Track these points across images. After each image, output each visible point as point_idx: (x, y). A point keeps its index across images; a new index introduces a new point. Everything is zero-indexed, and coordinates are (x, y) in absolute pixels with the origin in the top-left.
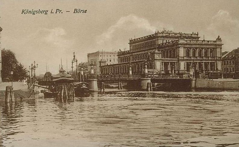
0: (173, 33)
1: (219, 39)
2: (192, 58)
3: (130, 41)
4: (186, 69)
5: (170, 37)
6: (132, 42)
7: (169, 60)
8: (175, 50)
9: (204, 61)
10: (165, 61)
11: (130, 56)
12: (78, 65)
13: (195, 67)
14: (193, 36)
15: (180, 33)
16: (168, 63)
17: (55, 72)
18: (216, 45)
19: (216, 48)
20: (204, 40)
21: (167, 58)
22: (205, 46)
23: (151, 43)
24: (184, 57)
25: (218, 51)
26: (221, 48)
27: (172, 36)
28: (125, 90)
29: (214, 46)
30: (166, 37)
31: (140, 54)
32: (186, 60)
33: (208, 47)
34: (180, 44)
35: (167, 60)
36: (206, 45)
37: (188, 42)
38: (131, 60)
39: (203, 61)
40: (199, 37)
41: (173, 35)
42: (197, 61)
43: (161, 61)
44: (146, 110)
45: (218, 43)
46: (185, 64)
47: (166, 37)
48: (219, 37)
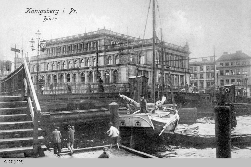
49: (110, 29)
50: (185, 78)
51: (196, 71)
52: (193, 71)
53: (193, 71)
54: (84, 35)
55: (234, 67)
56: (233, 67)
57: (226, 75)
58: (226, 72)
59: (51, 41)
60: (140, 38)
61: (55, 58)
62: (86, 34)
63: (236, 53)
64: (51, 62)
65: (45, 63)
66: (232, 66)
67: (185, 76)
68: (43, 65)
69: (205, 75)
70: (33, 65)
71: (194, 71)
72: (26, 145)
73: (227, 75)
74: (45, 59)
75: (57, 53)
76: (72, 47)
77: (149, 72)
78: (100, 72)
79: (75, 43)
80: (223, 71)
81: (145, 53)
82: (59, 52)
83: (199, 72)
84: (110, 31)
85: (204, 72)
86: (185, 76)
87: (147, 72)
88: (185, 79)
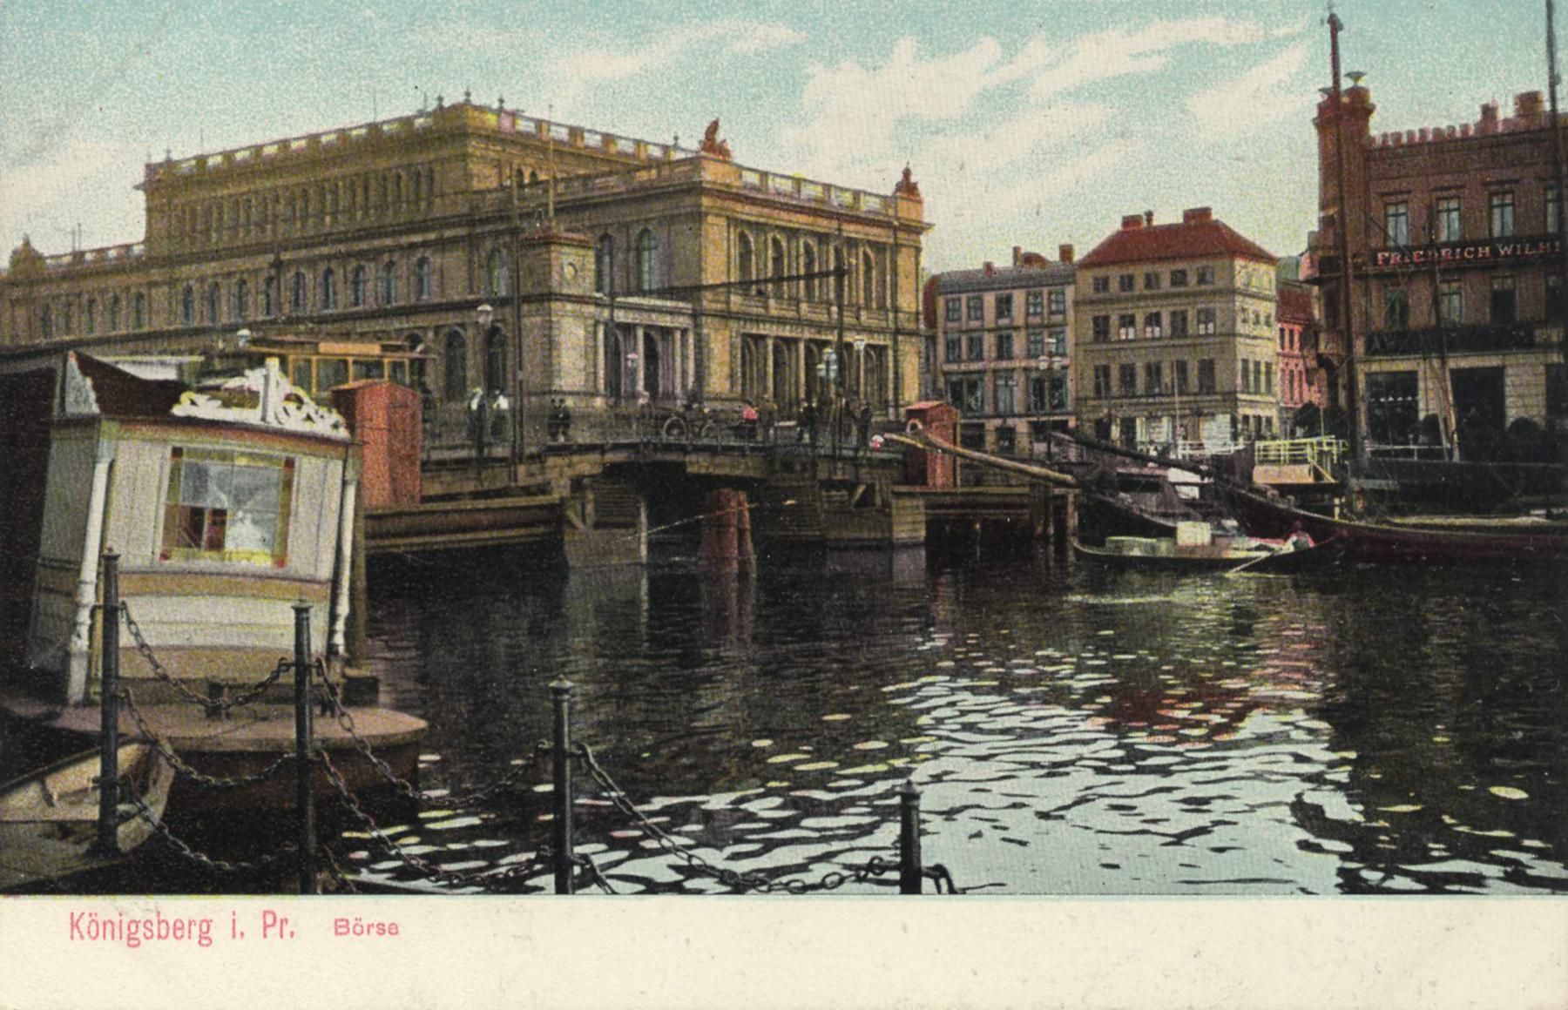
19: (896, 247)
26: (918, 250)
45: (905, 211)
48: (907, 173)
49: (501, 101)
50: (896, 361)
51: (1058, 312)
52: (964, 318)
53: (964, 318)
54: (369, 133)
55: (1214, 293)
56: (1153, 297)
57: (1146, 339)
58: (1123, 325)
59: (201, 160)
60: (676, 147)
61: (215, 256)
62: (374, 128)
63: (1181, 220)
64: (202, 279)
65: (172, 283)
66: (1203, 287)
67: (896, 351)
68: (159, 294)
69: (1019, 343)
70: (86, 297)
71: (1051, 313)
72: (597, 853)
73: (1128, 341)
74: (172, 261)
75: (234, 229)
76: (335, 192)
77: (678, 335)
78: (461, 331)
79: (322, 174)
80: (1106, 318)
81: (660, 234)
82: (242, 220)
83: (992, 325)
84: (500, 111)
85: (1015, 323)
86: (896, 351)
87: (667, 332)
88: (896, 366)
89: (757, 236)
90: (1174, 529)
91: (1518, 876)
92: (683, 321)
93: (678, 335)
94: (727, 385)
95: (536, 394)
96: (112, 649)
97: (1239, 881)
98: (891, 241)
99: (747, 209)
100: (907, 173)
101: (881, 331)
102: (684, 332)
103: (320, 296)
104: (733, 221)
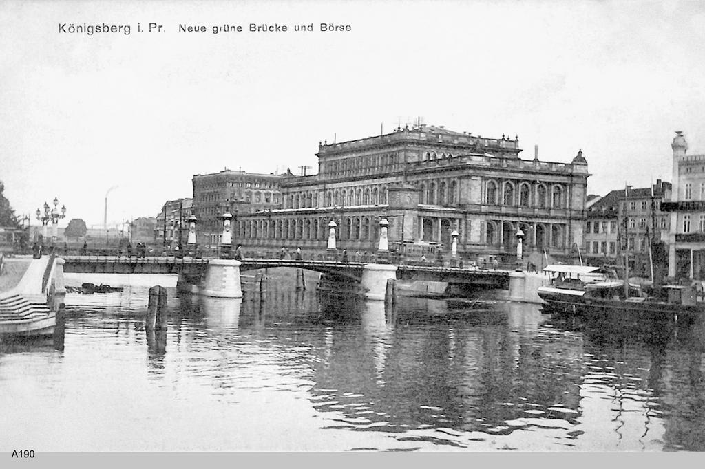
0: (448, 134)
1: (580, 159)
2: (503, 209)
3: (320, 146)
4: (485, 240)
5: (439, 145)
6: (327, 152)
7: (439, 211)
8: (454, 183)
9: (505, 219)
10: (428, 214)
11: (320, 190)
12: (445, 251)
13: (523, 240)
14: (503, 144)
15: (467, 134)
16: (437, 218)
17: (297, 172)
18: (571, 175)
19: (572, 185)
20: (536, 161)
21: (432, 203)
22: (541, 178)
23: (335, 165)
24: (480, 205)
25: (576, 192)
26: (585, 185)
27: (444, 142)
28: (428, 426)
29: (566, 178)
30: (428, 143)
31: (348, 188)
32: (486, 214)
33: (549, 179)
34: (470, 168)
35: (432, 211)
36: (542, 174)
37: (497, 161)
38: (321, 204)
39: (534, 220)
40: (520, 148)
41: (449, 138)
42: (500, 218)
43: (416, 212)
44: (373, 449)
45: (578, 169)
46: (482, 225)
47: (428, 143)
48: (580, 153)
89: (499, 183)
90: (449, 307)
91: (8, 205)
92: (460, 216)
93: (457, 221)
94: (479, 239)
95: (261, 285)
96: (80, 268)
97: (556, 428)
98: (569, 182)
99: (493, 173)
100: (580, 153)
101: (564, 218)
102: (460, 220)
103: (306, 235)
104: (484, 179)
